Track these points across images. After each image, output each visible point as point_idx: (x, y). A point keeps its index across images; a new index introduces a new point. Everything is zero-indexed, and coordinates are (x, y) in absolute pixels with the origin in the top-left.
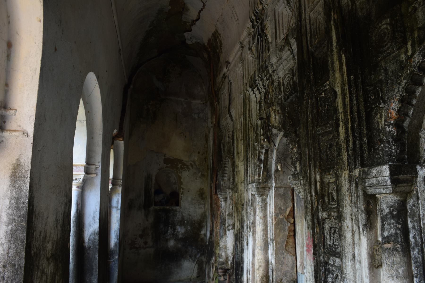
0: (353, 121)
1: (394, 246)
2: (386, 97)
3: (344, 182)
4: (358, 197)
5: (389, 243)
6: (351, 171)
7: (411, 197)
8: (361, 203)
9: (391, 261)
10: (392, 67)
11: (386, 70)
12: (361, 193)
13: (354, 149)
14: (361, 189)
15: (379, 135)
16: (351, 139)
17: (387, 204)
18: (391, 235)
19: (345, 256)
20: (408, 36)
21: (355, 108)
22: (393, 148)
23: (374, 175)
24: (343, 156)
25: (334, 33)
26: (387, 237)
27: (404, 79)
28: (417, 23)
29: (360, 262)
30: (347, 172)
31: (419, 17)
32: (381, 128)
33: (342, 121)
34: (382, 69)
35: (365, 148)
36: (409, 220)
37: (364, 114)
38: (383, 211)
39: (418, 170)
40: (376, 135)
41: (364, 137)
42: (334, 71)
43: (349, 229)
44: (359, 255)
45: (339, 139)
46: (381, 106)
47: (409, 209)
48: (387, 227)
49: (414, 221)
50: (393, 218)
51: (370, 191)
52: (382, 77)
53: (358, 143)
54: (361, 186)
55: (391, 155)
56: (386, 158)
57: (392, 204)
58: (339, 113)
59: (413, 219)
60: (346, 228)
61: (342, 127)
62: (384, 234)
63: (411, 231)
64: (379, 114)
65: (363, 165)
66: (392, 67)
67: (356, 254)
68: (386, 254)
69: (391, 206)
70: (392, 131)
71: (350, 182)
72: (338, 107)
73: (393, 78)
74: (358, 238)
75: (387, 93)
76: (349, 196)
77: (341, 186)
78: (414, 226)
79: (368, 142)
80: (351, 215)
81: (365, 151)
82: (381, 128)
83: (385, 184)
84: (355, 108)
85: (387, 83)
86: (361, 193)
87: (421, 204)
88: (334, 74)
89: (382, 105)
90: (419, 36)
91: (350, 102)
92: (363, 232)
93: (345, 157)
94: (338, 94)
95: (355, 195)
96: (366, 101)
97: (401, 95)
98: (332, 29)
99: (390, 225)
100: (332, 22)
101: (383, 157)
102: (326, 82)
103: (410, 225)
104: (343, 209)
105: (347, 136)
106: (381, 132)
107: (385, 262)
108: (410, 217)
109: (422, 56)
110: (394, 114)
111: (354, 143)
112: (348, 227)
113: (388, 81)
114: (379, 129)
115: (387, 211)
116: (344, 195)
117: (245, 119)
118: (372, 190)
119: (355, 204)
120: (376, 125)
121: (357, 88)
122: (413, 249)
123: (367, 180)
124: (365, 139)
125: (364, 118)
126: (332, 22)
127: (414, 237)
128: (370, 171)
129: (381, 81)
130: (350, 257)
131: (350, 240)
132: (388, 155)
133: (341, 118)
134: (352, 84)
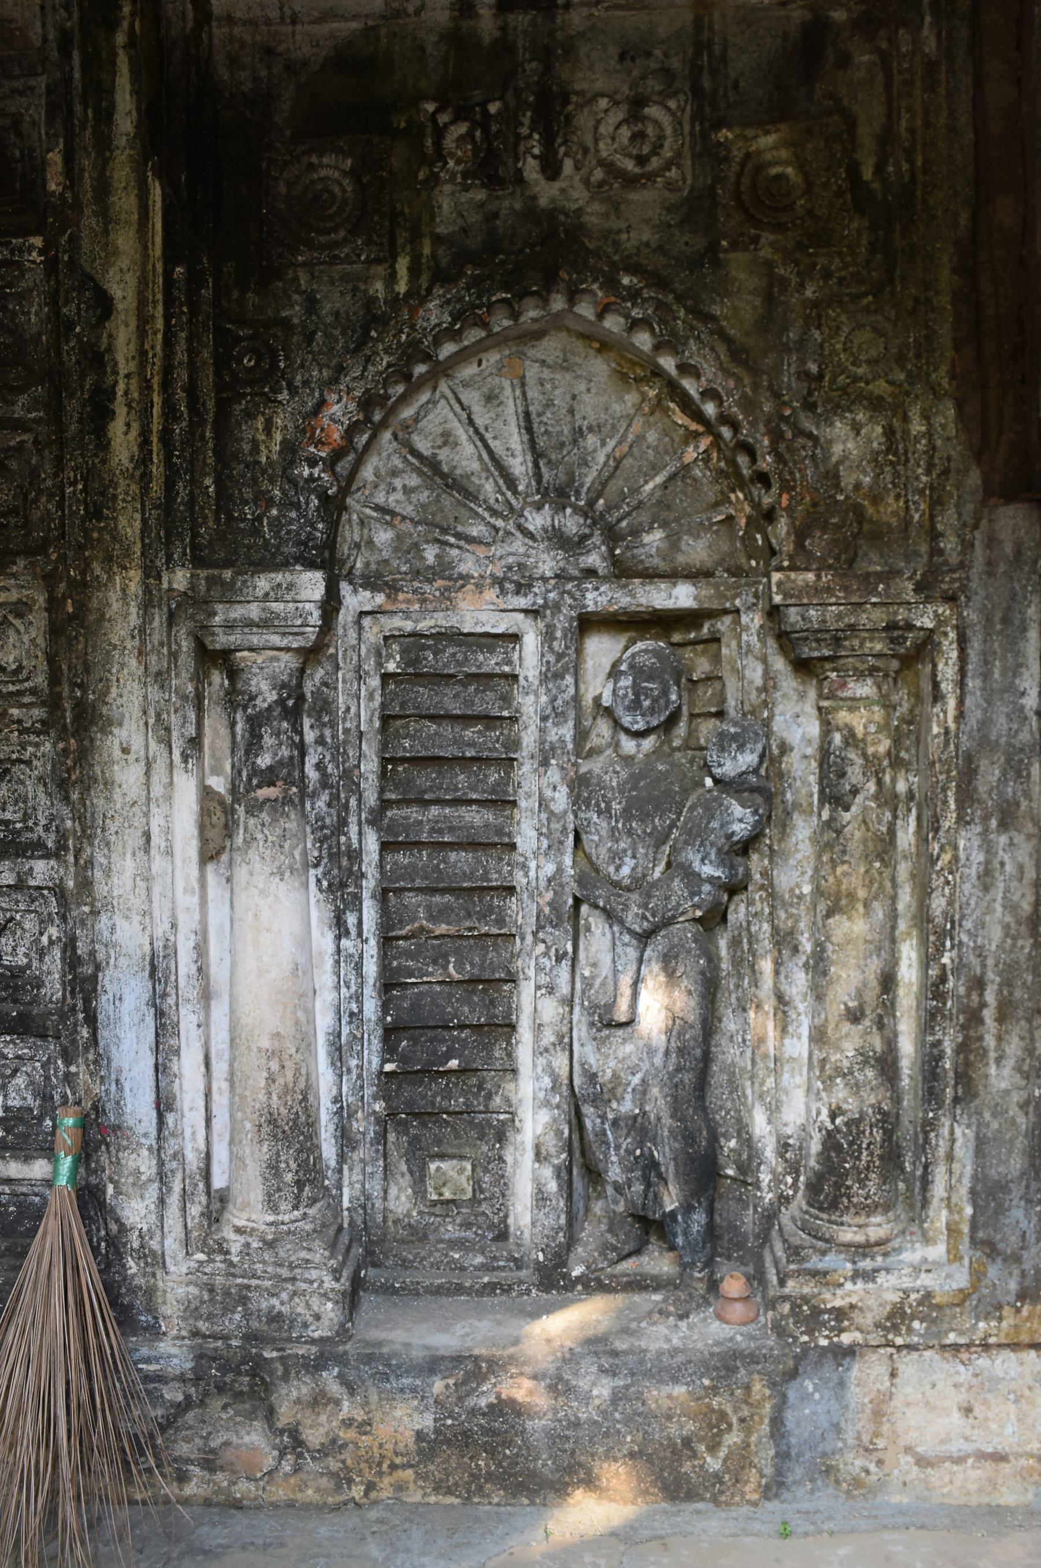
0: (170, 411)
1: (286, 791)
2: (299, 377)
3: (116, 606)
4: (174, 655)
5: (272, 784)
6: (150, 572)
7: (319, 663)
8: (184, 675)
9: (278, 831)
10: (333, 301)
11: (311, 303)
12: (186, 645)
13: (168, 506)
14: (189, 634)
15: (254, 479)
16: (157, 469)
17: (274, 678)
18: (281, 763)
19: (108, 844)
20: (400, 241)
21: (182, 375)
22: (320, 526)
23: (260, 593)
24: (122, 521)
25: (123, 81)
26: (270, 768)
27: (386, 351)
28: (432, 219)
29: (169, 852)
30: (135, 575)
31: (440, 207)
32: (264, 460)
33: (129, 405)
34: (296, 292)
35: (202, 508)
36: (307, 722)
37: (211, 404)
38: (260, 698)
39: (342, 593)
40: (244, 476)
41: (205, 475)
42: (106, 218)
43: (131, 757)
44: (168, 831)
45: (104, 462)
46: (280, 397)
47: (309, 695)
48: (268, 740)
49: (324, 725)
50: (285, 718)
51: (222, 640)
52: (295, 313)
53: (182, 491)
54: (190, 624)
55: (306, 545)
56: (290, 549)
57: (285, 678)
58: (115, 373)
59: (319, 718)
60: (117, 753)
61: (128, 425)
62: (259, 761)
63: (311, 750)
64: (261, 419)
65: (198, 562)
66: (333, 301)
67: (155, 831)
68: (264, 815)
69: (284, 686)
70: (319, 478)
71: (146, 606)
72: (110, 348)
73: (337, 332)
74: (166, 780)
75: (302, 366)
76: (140, 653)
77: (102, 618)
78: (322, 736)
79: (217, 492)
80: (145, 713)
81: (205, 517)
82: (264, 460)
83: (299, 622)
84: (182, 375)
85: (309, 338)
86: (184, 643)
87: (344, 681)
88: (106, 232)
89: (284, 396)
90: (434, 254)
91: (164, 350)
92: (186, 762)
93: (130, 525)
94: (120, 307)
95: (165, 650)
96: (221, 363)
97: (368, 390)
98: (113, 63)
99: (278, 735)
100: (120, 39)
101: (278, 547)
102: (26, 233)
103: (310, 736)
104: (106, 692)
105: (143, 460)
106: (264, 472)
107: (260, 836)
108: (309, 716)
109: (451, 314)
110: (336, 436)
111: (169, 485)
112: (126, 751)
113: (314, 333)
114: (259, 463)
115: (272, 697)
116: (115, 647)
117: (524, 394)
118: (232, 638)
119: (161, 678)
120: (246, 447)
121: (193, 313)
122: (314, 795)
123: (219, 607)
124: (208, 481)
125: (210, 417)
126: (120, 39)
127: (319, 766)
128: (244, 582)
129: (286, 324)
130: (133, 839)
131: (135, 789)
132: (300, 543)
133: (126, 393)
134: (176, 293)
